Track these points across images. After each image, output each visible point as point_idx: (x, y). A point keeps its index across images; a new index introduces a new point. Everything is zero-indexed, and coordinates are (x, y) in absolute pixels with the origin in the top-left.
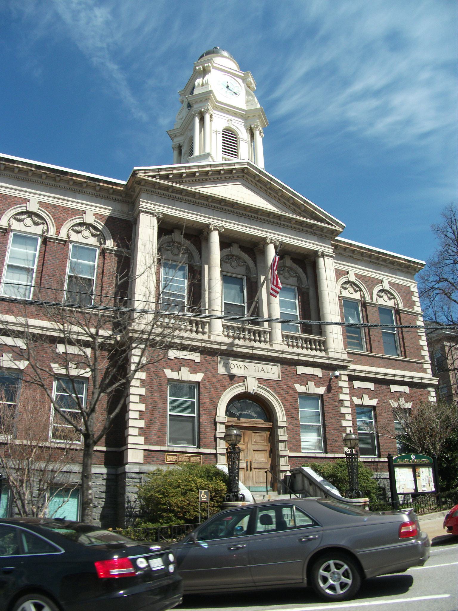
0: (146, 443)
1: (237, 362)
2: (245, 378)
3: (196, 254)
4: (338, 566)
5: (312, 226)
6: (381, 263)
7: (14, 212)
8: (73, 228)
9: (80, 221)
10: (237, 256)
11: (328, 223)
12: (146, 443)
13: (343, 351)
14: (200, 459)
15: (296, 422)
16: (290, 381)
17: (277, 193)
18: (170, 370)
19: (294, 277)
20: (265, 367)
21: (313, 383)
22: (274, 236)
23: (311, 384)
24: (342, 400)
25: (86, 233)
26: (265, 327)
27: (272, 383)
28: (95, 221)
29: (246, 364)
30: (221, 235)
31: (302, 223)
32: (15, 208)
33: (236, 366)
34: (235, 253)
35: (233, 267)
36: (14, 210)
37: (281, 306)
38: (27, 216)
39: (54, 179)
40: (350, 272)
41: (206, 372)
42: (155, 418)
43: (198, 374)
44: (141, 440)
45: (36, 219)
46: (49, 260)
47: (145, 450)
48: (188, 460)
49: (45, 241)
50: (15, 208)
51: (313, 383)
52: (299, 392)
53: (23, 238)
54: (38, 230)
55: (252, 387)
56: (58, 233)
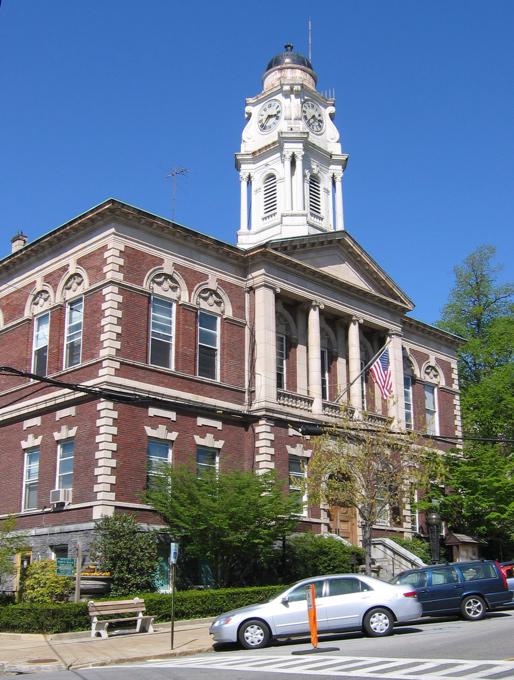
0: (117, 499)
3: (292, 325)
4: (470, 604)
5: (389, 303)
6: (432, 338)
11: (402, 302)
12: (117, 499)
13: (321, 412)
17: (363, 266)
22: (362, 315)
24: (113, 442)
26: (299, 392)
28: (162, 269)
30: (321, 313)
31: (381, 300)
37: (214, 337)
39: (185, 238)
44: (112, 496)
47: (116, 507)
52: (198, 445)
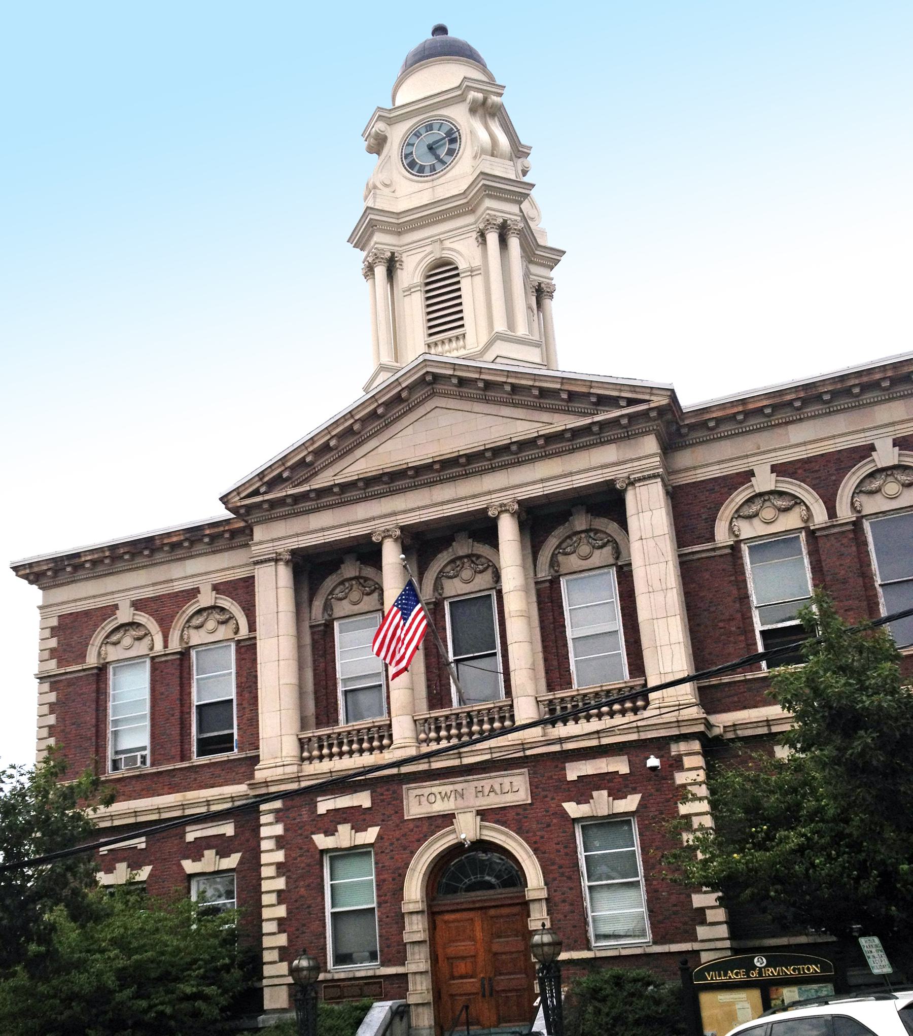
1: (441, 789)
2: (453, 816)
7: (103, 634)
8: (106, 642)
9: (868, 469)
10: (468, 556)
14: (381, 987)
15: (570, 884)
16: (553, 799)
18: (322, 835)
19: (601, 547)
20: (496, 783)
21: (605, 793)
23: (601, 796)
25: (892, 488)
27: (511, 814)
29: (459, 787)
32: (853, 473)
33: (438, 796)
34: (461, 553)
35: (467, 582)
36: (854, 478)
38: (122, 632)
40: (202, 590)
41: (382, 823)
42: (304, 925)
43: (369, 829)
45: (780, 503)
46: (162, 694)
48: (378, 990)
49: (812, 534)
50: (853, 473)
51: (605, 793)
53: (765, 547)
54: (142, 648)
55: (467, 829)
56: (832, 513)
